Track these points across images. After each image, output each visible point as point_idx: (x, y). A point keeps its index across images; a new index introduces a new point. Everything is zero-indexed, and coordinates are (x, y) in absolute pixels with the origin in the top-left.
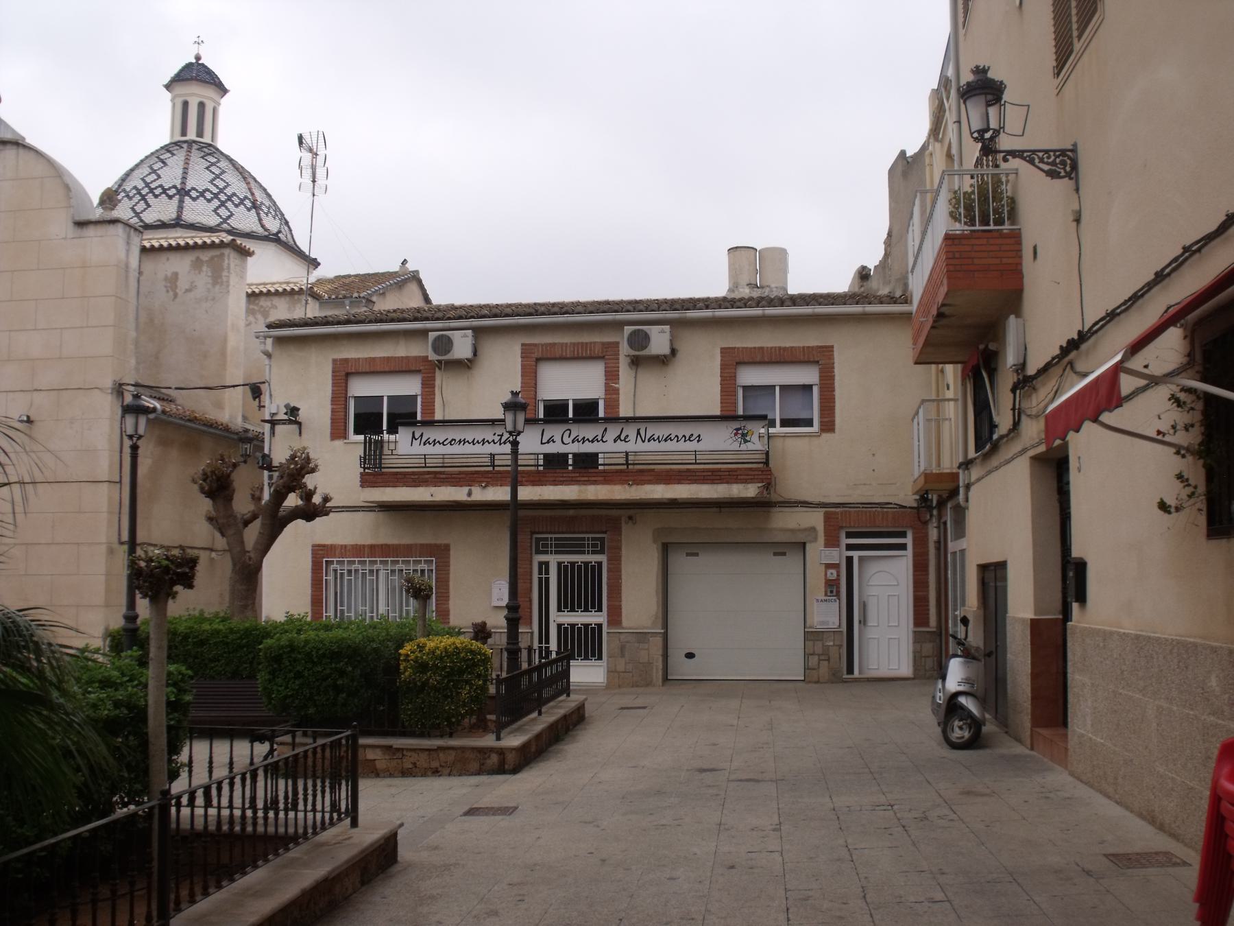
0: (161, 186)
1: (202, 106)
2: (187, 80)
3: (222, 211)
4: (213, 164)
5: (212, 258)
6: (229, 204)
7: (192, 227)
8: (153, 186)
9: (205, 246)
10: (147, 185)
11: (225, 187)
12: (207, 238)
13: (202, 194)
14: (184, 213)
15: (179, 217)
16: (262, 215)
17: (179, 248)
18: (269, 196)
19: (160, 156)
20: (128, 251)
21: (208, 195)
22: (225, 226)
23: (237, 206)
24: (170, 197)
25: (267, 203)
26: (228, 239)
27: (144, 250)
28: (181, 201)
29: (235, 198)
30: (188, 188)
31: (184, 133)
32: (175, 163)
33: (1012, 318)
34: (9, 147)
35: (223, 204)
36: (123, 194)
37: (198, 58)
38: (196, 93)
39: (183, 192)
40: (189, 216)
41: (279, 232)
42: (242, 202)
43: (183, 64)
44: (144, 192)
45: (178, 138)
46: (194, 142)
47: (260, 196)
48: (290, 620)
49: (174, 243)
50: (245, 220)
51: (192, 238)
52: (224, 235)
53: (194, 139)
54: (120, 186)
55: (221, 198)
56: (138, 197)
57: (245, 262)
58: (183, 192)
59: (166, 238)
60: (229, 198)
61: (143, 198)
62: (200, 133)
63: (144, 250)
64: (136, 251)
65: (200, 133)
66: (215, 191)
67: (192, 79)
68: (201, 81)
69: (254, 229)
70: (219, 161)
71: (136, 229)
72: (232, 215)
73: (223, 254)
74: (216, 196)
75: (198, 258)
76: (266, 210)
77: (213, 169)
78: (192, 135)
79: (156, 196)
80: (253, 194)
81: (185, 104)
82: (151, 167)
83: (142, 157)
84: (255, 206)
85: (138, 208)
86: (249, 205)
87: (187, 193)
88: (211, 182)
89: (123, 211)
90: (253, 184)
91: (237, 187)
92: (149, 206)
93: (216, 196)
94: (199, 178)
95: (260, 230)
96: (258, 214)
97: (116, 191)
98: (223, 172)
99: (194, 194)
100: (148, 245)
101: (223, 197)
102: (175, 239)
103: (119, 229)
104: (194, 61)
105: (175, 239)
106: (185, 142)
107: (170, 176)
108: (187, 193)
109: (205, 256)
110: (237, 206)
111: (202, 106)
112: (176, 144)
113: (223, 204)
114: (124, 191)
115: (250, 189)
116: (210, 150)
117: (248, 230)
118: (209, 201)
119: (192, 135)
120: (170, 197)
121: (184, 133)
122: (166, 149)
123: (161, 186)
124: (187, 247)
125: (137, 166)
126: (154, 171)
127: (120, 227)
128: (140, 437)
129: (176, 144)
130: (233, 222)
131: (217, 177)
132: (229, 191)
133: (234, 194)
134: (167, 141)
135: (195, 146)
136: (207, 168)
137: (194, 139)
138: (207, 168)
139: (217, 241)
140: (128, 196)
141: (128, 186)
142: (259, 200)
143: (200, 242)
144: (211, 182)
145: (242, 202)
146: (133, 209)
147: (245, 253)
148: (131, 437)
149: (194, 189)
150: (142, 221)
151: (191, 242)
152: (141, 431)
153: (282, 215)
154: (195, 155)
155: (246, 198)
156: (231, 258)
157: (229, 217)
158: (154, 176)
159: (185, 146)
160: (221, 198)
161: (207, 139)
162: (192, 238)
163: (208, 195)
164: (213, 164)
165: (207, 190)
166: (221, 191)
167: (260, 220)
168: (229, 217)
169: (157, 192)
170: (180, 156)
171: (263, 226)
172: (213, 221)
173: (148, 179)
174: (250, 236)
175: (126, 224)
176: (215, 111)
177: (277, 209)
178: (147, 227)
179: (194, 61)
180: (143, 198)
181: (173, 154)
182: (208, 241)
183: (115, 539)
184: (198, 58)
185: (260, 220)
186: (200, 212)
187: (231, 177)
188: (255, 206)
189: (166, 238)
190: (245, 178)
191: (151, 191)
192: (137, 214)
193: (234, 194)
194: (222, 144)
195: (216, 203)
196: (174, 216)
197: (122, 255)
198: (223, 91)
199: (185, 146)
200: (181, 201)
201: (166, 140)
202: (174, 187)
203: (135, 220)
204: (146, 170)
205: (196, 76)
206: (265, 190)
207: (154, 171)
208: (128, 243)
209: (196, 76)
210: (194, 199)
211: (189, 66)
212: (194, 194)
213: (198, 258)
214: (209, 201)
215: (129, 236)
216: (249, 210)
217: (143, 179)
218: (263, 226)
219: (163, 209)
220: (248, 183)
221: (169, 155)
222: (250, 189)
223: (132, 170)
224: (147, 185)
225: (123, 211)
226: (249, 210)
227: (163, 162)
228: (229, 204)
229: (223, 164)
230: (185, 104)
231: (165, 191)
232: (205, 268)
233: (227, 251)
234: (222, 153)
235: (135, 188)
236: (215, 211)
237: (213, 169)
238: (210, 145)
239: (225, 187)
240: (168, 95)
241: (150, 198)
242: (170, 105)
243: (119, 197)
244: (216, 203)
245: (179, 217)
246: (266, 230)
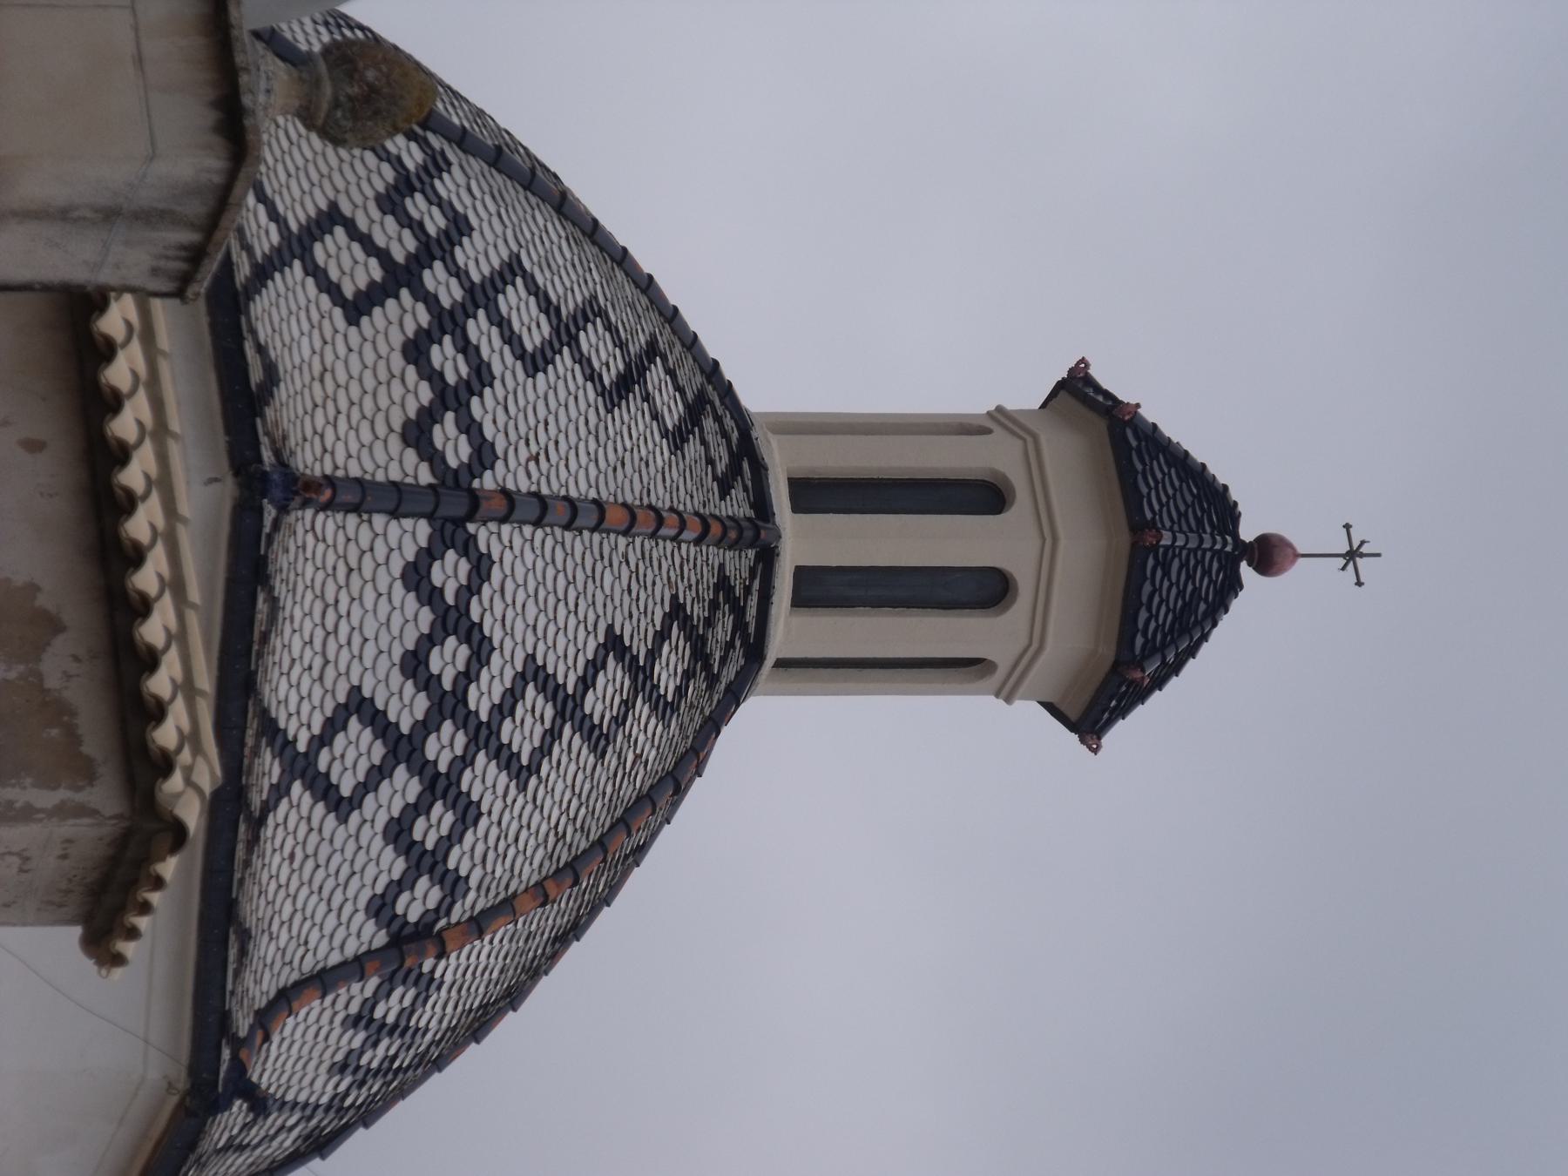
0: (481, 375)
1: (988, 590)
2: (1132, 499)
3: (353, 753)
4: (640, 674)
5: (59, 711)
6: (404, 786)
7: (248, 574)
8: (479, 329)
9: (128, 661)
10: (482, 296)
11: (506, 758)
12: (181, 677)
13: (453, 620)
14: (328, 524)
15: (303, 491)
16: (356, 993)
17: (105, 504)
18: (478, 1024)
19: (658, 359)
20: (64, 215)
21: (448, 659)
22: (269, 768)
23: (398, 832)
24: (417, 434)
25: (434, 1016)
26: (187, 797)
27: (79, 306)
28: (395, 500)
29: (442, 818)
30: (485, 535)
31: (814, 494)
32: (619, 454)
33: (425, 325)
35: (403, 748)
36: (413, 156)
37: (1269, 554)
38: (1060, 551)
39: (454, 506)
40: (311, 548)
41: (260, 1104)
42: (426, 862)
43: (1221, 471)
44: (436, 278)
45: (782, 462)
46: (767, 557)
47: (468, 967)
49: (133, 476)
50: (315, 885)
51: (176, 585)
52: (209, 773)
53: (786, 553)
54: (462, 139)
55: (436, 738)
56: (402, 245)
57: (51, 910)
58: (454, 506)
59: (160, 431)
60: (440, 786)
61: (401, 277)
62: (822, 589)
63: (79, 306)
64: (68, 260)
65: (822, 589)
66: (481, 699)
67: (1139, 526)
69: (264, 949)
70: (663, 708)
71: (196, 256)
72: (342, 807)
73: (85, 772)
74: (448, 704)
75: (52, 625)
76: (389, 1010)
77: (613, 679)
79: (416, 351)
80: (478, 925)
81: (987, 496)
82: (590, 312)
83: (646, 262)
84: (406, 947)
85: (335, 252)
86: (418, 902)
87: (450, 533)
88: (534, 673)
89: (300, 168)
90: (544, 920)
91: (514, 830)
92: (357, 308)
93: (448, 704)
94: (544, 600)
95: (259, 983)
96: (356, 967)
97: (430, 121)
98: (598, 739)
99: (449, 572)
100: (115, 320)
101: (443, 746)
102: (163, 482)
103: (190, 161)
104: (1248, 532)
105: (163, 482)
106: (762, 506)
107: (546, 428)
108: (450, 533)
109: (69, 669)
110: (398, 832)
111: (988, 590)
113: (403, 748)
114: (436, 165)
115: (506, 907)
116: (721, 655)
117: (254, 910)
118: (414, 664)
119: (804, 541)
120: (417, 434)
121: (814, 494)
122: (711, 396)
123: (481, 375)
124: (112, 557)
125: (591, 232)
126: (565, 333)
127: (208, 164)
129: (745, 455)
130: (295, 817)
131: (568, 707)
132: (484, 779)
133: (468, 814)
134: (753, 399)
135: (738, 564)
136: (614, 644)
137: (786, 553)
138: (614, 644)
139: (166, 735)
140: (405, 185)
141: (462, 184)
142: (448, 969)
143: (153, 631)
144: (534, 673)
145: (426, 862)
146: (331, 218)
147: (104, 912)
149: (481, 567)
150: (263, 273)
151: (146, 579)
153: (367, 1115)
155: (454, 885)
156: (63, 824)
157: (325, 790)
158: (535, 331)
159: (737, 505)
160: (436, 738)
161: (790, 630)
162: (187, 687)
163: (448, 659)
164: (640, 674)
165: (481, 651)
166: (483, 736)
167: (323, 980)
168: (325, 790)
169: (444, 356)
170: (676, 481)
171: (286, 999)
172: (295, 695)
173: (514, 300)
174: (221, 926)
175: (222, 201)
177: (398, 1082)
178: (228, 312)
179: (1248, 532)
180: (401, 277)
181: (677, 439)
182: (160, 683)
184: (1269, 554)
185: (323, 980)
186: (343, 611)
188: (406, 947)
189: (160, 431)
190: (571, 870)
191: (448, 322)
192: (298, 246)
193: (468, 814)
194: (767, 723)
195: (406, 706)
196: (308, 461)
197: (37, 187)
198: (1092, 713)
199: (737, 505)
200: (395, 500)
201: (760, 391)
202: (484, 455)
203: (265, 237)
204: (568, 291)
206: (512, 997)
207: (565, 333)
208: (109, 215)
210: (416, 576)
211: (1217, 506)
212: (449, 572)
213: (52, 625)
214: (414, 664)
215: (148, 217)
216: (380, 908)
217: (512, 269)
218: (286, 999)
219: (341, 391)
220: (541, 893)
221: (673, 413)
222: (506, 907)
223: (562, 204)
224: (482, 296)
225: (300, 168)
226: (380, 908)
227: (627, 383)
228: (404, 786)
229: (648, 737)
230: (987, 496)
231: (451, 399)
233: (105, 796)
234: (713, 725)
235: (459, 226)
236: (359, 706)
237: (613, 679)
238: (755, 653)
239: (506, 758)
240: (1028, 391)
241: (403, 316)
242: (976, 404)
243: (398, 144)
244: (406, 706)
245: (303, 491)
246: (265, 1019)
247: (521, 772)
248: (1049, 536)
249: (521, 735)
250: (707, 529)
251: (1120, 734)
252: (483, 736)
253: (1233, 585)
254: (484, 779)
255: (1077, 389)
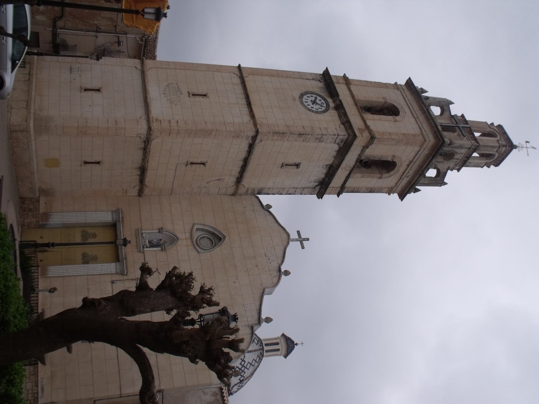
1: (278, 350)
5: (218, 400)
11: (247, 368)
21: (243, 363)
31: (267, 345)
34: (251, 330)
37: (296, 344)
38: (283, 347)
45: (264, 343)
46: (263, 350)
48: (82, 236)
62: (267, 351)
65: (267, 351)
66: (245, 365)
67: (288, 345)
68: (288, 348)
75: (217, 394)
78: (266, 348)
81: (277, 344)
86: (241, 379)
88: (249, 363)
98: (253, 366)
106: (263, 346)
111: (278, 350)
112: (262, 343)
119: (266, 348)
121: (267, 345)
128: (143, 15)
132: (246, 370)
133: (245, 372)
135: (261, 351)
148: (143, 10)
152: (146, 16)
154: (258, 353)
155: (244, 377)
159: (261, 347)
161: (265, 354)
163: (243, 363)
164: (256, 361)
166: (246, 367)
167: (236, 385)
171: (233, 386)
176: (278, 355)
183: (96, 399)
184: (296, 344)
185: (236, 385)
187: (252, 369)
198: (286, 356)
199: (261, 347)
201: (261, 338)
205: (290, 345)
209: (290, 345)
211: (293, 342)
213: (217, 394)
218: (233, 386)
229: (256, 364)
230: (277, 344)
232: (214, 398)
242: (276, 336)
247: (248, 369)
248: (282, 346)
249: (248, 367)
250: (259, 350)
251: (288, 357)
252: (246, 367)
253: (294, 347)
254: (246, 370)
255: (283, 335)
